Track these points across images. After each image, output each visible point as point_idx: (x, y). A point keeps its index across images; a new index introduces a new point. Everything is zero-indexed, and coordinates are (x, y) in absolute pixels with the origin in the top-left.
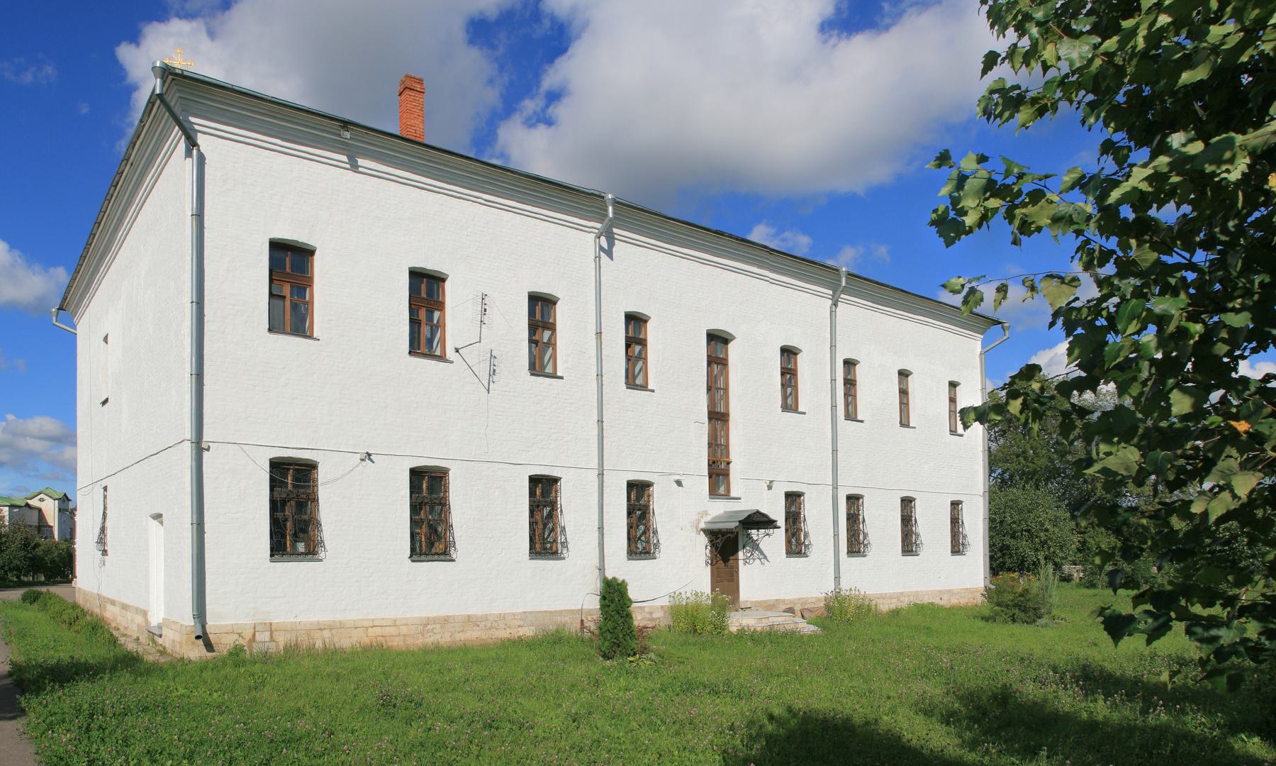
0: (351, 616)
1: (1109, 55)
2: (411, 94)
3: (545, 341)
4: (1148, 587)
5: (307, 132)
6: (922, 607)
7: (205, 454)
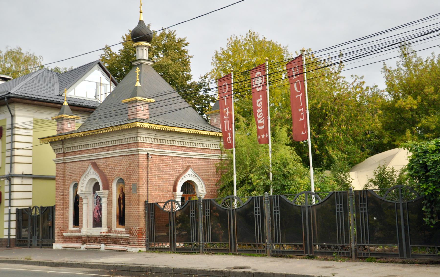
0: (194, 255)
2: (87, 172)
3: (133, 64)
5: (399, 233)
6: (106, 238)
7: (24, 173)
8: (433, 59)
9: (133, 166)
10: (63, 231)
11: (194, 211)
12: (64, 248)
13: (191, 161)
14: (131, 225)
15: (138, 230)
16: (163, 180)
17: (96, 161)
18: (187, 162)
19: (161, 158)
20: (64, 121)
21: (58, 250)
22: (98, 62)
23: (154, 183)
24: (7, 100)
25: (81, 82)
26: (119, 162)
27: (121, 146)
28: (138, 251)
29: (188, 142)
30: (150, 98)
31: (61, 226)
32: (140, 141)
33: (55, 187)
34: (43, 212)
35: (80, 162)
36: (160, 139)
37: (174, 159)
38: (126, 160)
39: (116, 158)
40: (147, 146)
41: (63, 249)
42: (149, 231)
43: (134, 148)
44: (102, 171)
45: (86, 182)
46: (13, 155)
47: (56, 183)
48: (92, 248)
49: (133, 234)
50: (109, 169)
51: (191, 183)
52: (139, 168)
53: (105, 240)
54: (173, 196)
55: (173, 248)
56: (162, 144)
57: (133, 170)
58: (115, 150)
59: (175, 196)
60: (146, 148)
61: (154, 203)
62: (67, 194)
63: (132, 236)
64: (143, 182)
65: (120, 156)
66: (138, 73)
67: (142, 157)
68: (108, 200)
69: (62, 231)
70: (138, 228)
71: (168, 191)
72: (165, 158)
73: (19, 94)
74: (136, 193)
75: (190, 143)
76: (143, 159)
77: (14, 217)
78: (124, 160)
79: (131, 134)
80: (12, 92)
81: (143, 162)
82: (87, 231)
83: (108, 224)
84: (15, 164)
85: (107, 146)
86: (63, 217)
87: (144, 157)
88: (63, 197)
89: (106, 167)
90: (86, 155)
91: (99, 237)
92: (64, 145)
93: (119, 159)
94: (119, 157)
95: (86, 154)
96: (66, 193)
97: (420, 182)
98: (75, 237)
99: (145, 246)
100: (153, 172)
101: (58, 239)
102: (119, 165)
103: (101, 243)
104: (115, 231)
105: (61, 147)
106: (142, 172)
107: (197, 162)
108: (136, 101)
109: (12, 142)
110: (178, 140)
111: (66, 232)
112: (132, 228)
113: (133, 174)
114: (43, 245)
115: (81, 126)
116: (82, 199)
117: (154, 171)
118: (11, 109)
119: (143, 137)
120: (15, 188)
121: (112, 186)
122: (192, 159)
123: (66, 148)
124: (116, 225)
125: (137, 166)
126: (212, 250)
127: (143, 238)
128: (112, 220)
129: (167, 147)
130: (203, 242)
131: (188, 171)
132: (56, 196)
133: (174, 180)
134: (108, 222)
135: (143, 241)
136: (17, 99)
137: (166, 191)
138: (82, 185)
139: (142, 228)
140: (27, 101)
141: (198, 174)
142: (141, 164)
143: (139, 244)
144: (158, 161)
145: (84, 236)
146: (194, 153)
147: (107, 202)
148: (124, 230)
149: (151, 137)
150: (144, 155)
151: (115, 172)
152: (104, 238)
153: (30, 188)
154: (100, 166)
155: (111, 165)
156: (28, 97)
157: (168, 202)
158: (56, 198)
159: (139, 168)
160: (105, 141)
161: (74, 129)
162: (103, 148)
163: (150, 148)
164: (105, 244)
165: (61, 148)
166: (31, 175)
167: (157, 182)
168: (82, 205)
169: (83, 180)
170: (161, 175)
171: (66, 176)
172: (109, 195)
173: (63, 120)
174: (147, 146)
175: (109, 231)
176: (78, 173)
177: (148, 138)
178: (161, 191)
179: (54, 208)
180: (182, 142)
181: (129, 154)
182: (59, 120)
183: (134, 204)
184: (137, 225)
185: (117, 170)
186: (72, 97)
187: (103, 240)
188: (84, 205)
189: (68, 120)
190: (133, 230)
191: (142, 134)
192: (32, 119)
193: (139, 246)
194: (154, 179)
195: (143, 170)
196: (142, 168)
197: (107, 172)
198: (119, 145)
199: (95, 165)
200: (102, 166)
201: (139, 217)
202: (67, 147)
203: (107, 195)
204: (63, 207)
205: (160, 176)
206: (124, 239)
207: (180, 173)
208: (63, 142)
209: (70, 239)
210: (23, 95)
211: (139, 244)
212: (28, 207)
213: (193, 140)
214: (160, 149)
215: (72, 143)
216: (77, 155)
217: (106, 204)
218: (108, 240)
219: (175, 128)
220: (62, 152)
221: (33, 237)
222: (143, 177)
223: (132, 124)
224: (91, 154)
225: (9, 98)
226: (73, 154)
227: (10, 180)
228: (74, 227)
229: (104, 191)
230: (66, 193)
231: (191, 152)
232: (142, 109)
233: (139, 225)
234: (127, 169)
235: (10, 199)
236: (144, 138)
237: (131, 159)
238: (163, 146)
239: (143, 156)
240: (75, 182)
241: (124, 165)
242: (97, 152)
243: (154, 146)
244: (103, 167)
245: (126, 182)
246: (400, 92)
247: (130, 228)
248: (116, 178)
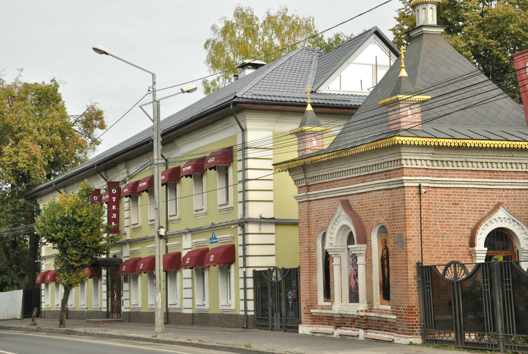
1: (253, 25)
2: (337, 216)
4: (23, 166)
5: (461, 286)
6: (366, 320)
9: (398, 207)
10: (311, 306)
11: (487, 281)
12: (313, 333)
13: (504, 195)
14: (397, 300)
15: (407, 310)
16: (449, 228)
17: (348, 197)
18: (497, 196)
19: (445, 192)
20: (307, 136)
21: (305, 336)
22: (374, 31)
23: (433, 233)
24: (233, 107)
25: (347, 66)
26: (379, 200)
27: (380, 175)
28: (408, 343)
29: (496, 163)
30: (418, 95)
31: (308, 298)
32: (405, 166)
33: (298, 239)
34: (285, 276)
35: (329, 200)
36: (442, 161)
37: (470, 192)
38: (388, 196)
39: (374, 193)
40: (419, 172)
41: (311, 334)
42: (425, 312)
43: (397, 177)
44: (357, 214)
45: (336, 232)
46: (246, 189)
47: (300, 233)
48: (348, 336)
49: (402, 315)
50: (366, 210)
51: (504, 232)
52: (405, 209)
53: (365, 323)
54: (471, 255)
55: (459, 342)
56: (446, 168)
57: (398, 213)
58: (373, 180)
59: (473, 255)
60: (416, 176)
61: (430, 266)
62: (314, 249)
63: (400, 318)
64: (412, 232)
65: (380, 190)
66: (403, 55)
67: (410, 191)
68: (366, 260)
69: (310, 306)
70: (408, 307)
71: (460, 246)
72: (453, 192)
73: (249, 97)
74: (403, 249)
75: (501, 163)
76: (412, 194)
77: (250, 283)
78: (386, 196)
79: (392, 156)
80: (239, 95)
81: (412, 200)
82: (340, 308)
83: (367, 298)
84: (249, 203)
85: (362, 174)
86: (310, 285)
87: (415, 191)
88: (309, 255)
89: (362, 208)
90: (334, 189)
91: (356, 319)
92: (307, 174)
93: (378, 194)
94: (378, 193)
95: (335, 187)
96: (313, 248)
98: (326, 317)
99: (421, 336)
100: (432, 216)
101: (305, 318)
102: (379, 204)
103: (359, 328)
104: (377, 309)
105: (302, 176)
106: (411, 215)
107: (516, 196)
108: (397, 101)
109: (245, 169)
110: (477, 160)
111: (315, 309)
112: (400, 306)
113: (398, 219)
114: (287, 327)
115: (331, 144)
116: (332, 258)
117: (433, 213)
118: (240, 121)
119: (411, 160)
120: (250, 239)
121: (370, 238)
122: (506, 192)
123: (309, 178)
124: (379, 301)
125: (403, 206)
126: (518, 347)
127: (416, 322)
128: (372, 292)
129: (457, 172)
130: (502, 333)
131: (496, 212)
132: (300, 253)
133: (471, 227)
134: (367, 295)
135: (417, 328)
136: (247, 105)
137: (456, 246)
138: (331, 236)
139: (414, 306)
140: (261, 107)
141: (518, 216)
142: (409, 203)
143: (410, 331)
144: (439, 197)
145: (336, 316)
146: (509, 181)
147: (365, 263)
148: (388, 308)
149: (425, 158)
150: (414, 189)
151: (373, 215)
152: (362, 320)
153: (271, 239)
154: (354, 206)
155: (368, 204)
156: (262, 99)
157: (449, 265)
158: (300, 255)
159: (405, 209)
160: (359, 166)
161: (322, 148)
162: (357, 177)
163: (424, 176)
164: (364, 329)
165: (304, 179)
166: (273, 218)
167: (439, 230)
168: (333, 267)
169: (332, 228)
170: (446, 219)
171: (312, 222)
172: (367, 252)
173: (305, 135)
174: (419, 172)
175: (369, 309)
176: (326, 217)
177: (420, 160)
178: (447, 246)
179: (298, 269)
180: (484, 164)
181: (391, 187)
182: (300, 134)
183: (400, 267)
184: (405, 300)
185: (377, 212)
186: (337, 93)
187: (362, 323)
188: (335, 267)
189: (313, 135)
190: (401, 309)
191: (407, 154)
192: (270, 133)
193: (410, 334)
194: (434, 227)
195: (412, 212)
196: (411, 209)
197: (364, 216)
198: (378, 173)
199: (347, 205)
200: (356, 206)
201: (408, 288)
202: (311, 176)
203: (365, 252)
204: (310, 270)
205: (444, 222)
206: (390, 322)
207: (483, 216)
208: (304, 168)
209: (320, 319)
210: (254, 97)
211: (411, 333)
212: (266, 269)
213: (506, 158)
214: (442, 177)
215: (316, 171)
216: (325, 189)
217: (364, 266)
218: (369, 323)
219: (466, 141)
220: (305, 184)
221: (275, 313)
222: (412, 224)
223: (389, 140)
224: (341, 188)
225: (235, 104)
226: (319, 187)
227: (243, 227)
228: (325, 301)
229: (359, 246)
230: (313, 248)
231: (503, 179)
232: (410, 112)
233: (408, 300)
234: (390, 211)
235: (245, 256)
236: (413, 161)
237: (394, 195)
238: (449, 172)
239: (412, 190)
240: (382, 225)
241: (385, 205)
242: (349, 185)
243: (432, 173)
244: (358, 208)
245: (390, 231)
247: (397, 306)
248: (376, 225)
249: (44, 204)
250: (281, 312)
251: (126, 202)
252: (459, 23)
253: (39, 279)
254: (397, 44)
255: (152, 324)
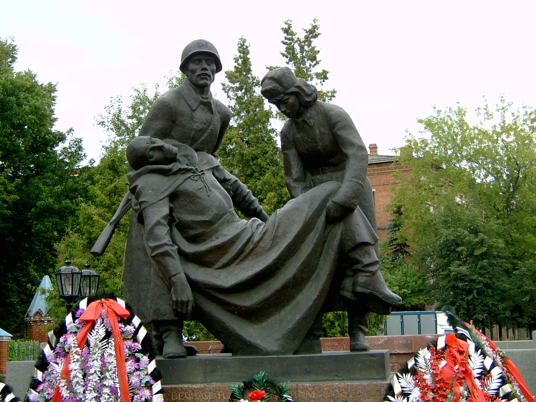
8: (153, 385)
97: (506, 316)
246: (354, 284)
249: (73, 382)
250: (87, 267)
251: (156, 393)
252: (32, 210)
253: (350, 202)
254: (8, 101)
255: (385, 356)
